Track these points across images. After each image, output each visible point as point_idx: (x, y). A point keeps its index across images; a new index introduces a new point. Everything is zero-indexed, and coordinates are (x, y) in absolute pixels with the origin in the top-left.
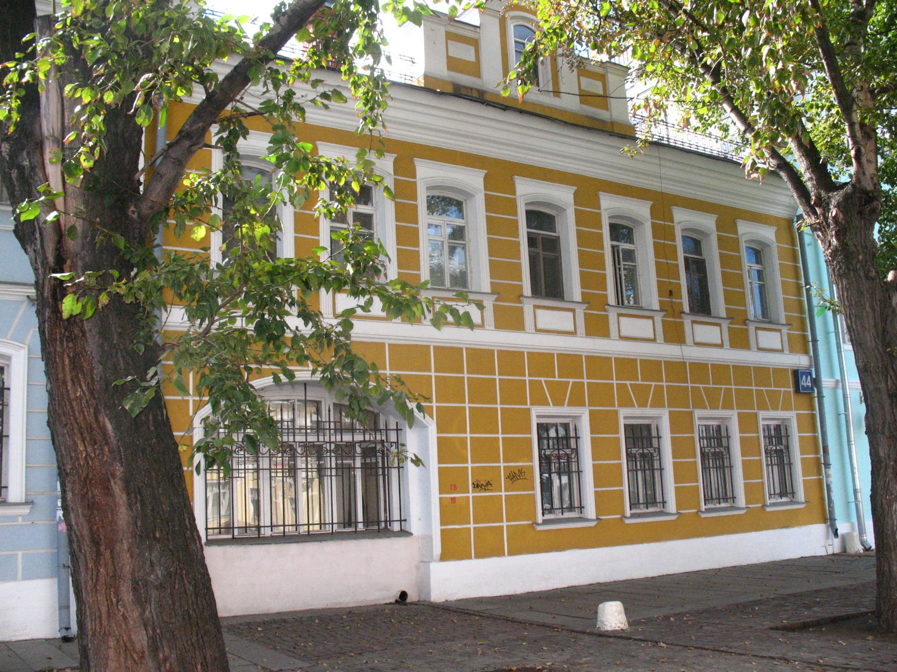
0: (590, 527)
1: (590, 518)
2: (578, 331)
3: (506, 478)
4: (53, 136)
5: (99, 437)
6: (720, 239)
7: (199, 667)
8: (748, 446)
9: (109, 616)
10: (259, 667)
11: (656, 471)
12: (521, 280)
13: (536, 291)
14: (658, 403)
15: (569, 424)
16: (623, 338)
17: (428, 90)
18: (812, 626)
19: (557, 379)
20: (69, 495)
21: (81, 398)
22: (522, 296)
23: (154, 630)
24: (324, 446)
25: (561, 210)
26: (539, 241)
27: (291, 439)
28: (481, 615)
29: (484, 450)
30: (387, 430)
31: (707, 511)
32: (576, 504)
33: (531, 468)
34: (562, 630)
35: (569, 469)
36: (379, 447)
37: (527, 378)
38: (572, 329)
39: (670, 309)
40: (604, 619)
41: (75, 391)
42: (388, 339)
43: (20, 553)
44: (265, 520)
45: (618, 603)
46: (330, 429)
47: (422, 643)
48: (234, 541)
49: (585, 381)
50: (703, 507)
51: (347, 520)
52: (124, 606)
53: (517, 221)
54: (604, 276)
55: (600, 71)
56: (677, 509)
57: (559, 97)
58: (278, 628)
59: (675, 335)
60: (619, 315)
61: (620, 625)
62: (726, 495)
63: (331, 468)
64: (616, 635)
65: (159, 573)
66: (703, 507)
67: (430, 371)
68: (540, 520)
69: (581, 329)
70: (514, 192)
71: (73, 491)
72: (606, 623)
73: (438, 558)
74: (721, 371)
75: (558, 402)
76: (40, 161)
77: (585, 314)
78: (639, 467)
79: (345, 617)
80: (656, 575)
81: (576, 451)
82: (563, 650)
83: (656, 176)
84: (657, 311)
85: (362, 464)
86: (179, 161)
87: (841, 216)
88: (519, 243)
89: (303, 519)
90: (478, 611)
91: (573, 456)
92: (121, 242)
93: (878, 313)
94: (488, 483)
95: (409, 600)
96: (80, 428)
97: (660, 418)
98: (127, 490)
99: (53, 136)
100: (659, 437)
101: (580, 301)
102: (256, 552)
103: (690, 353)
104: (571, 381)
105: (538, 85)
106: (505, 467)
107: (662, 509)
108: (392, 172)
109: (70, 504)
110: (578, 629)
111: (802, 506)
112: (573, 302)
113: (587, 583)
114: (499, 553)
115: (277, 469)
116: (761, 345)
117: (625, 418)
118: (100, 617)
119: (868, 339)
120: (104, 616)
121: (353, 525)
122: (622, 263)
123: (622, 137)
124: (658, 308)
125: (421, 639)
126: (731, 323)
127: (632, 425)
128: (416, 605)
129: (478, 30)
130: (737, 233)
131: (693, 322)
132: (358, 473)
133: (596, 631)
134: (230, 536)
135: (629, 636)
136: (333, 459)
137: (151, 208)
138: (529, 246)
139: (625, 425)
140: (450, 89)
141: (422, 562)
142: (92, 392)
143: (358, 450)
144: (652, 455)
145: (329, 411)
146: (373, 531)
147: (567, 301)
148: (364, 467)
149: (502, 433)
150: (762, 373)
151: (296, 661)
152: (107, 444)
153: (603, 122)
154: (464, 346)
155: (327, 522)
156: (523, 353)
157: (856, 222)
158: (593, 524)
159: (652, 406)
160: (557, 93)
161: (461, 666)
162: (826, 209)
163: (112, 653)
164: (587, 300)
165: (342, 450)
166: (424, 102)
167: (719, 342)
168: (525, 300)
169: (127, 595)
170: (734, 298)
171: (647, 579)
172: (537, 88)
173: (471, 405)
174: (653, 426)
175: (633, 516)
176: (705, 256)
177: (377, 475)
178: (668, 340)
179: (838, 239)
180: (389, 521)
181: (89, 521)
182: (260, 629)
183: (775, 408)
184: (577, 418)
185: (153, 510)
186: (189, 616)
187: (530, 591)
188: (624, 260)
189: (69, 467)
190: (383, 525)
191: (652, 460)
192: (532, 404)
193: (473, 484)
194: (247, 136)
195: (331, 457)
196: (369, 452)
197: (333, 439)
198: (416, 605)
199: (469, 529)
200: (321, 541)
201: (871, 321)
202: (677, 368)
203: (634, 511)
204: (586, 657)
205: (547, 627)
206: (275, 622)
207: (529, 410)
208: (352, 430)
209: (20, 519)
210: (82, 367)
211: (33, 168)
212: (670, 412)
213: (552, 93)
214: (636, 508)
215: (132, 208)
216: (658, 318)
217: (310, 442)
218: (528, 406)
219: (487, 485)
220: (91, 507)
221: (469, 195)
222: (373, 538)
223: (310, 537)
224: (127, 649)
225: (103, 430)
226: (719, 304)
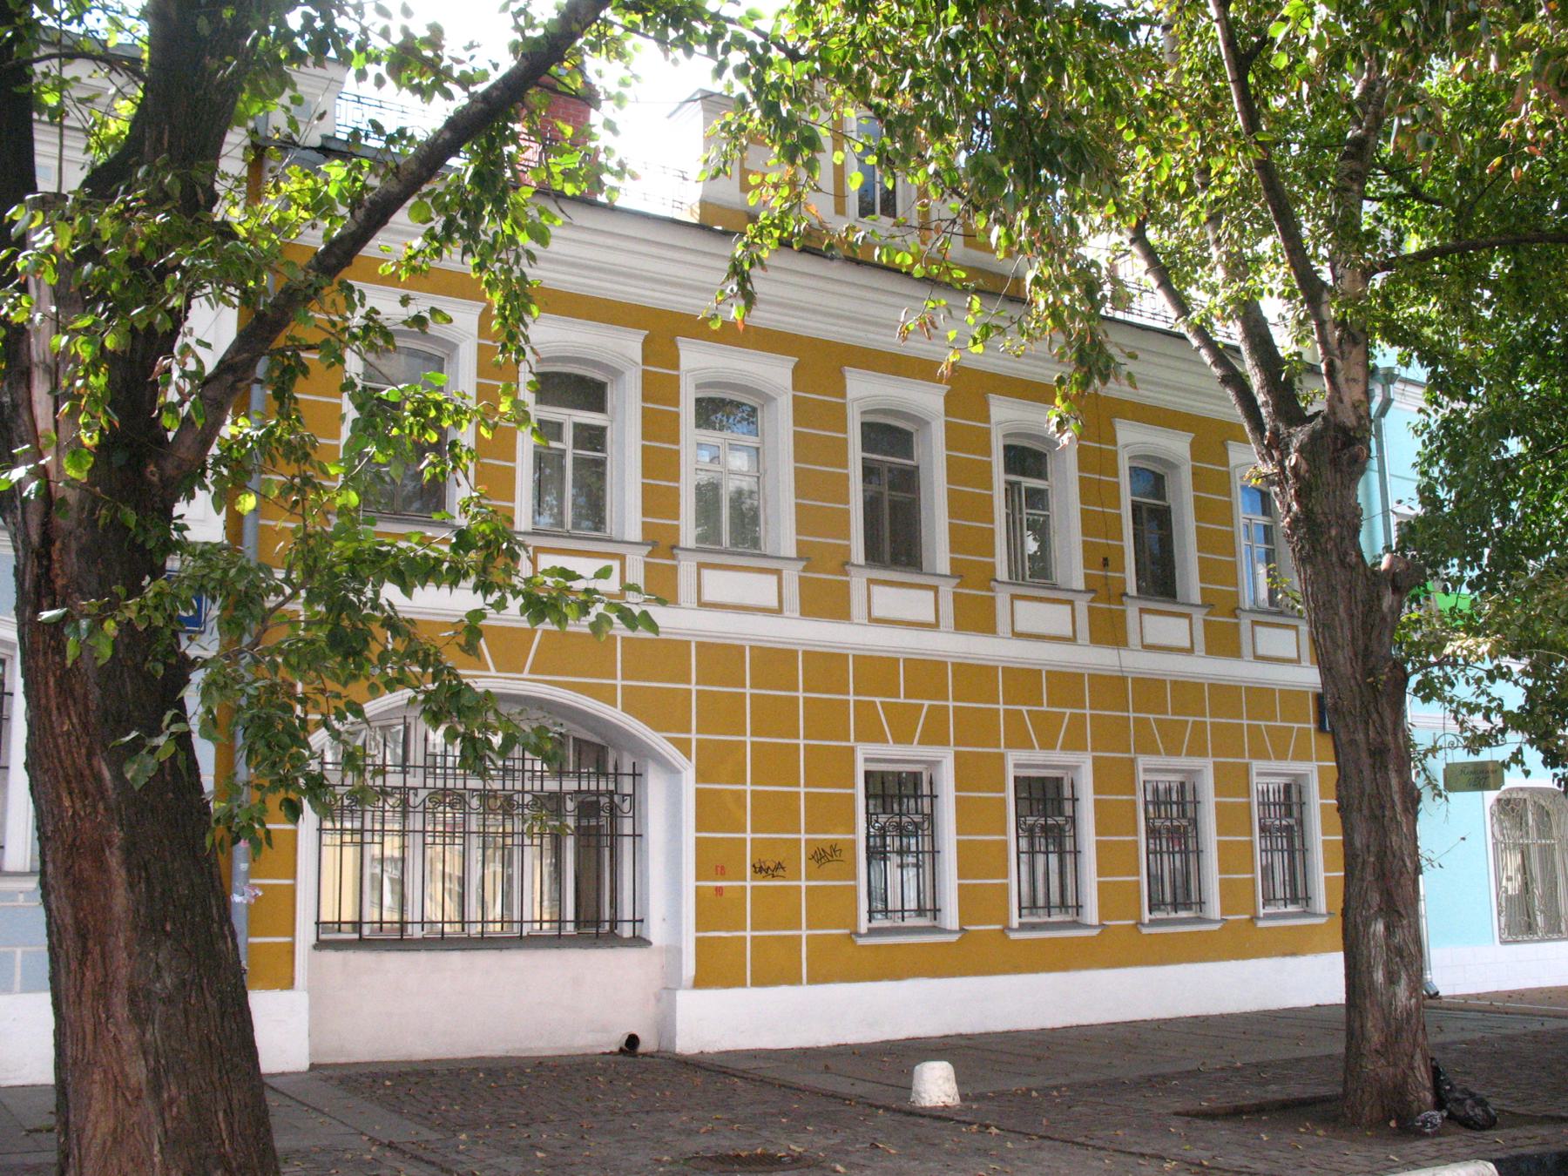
0: (949, 944)
2: (942, 624)
3: (811, 858)
4: (44, 362)
5: (91, 787)
6: (1196, 473)
7: (221, 1115)
8: (1229, 819)
9: (95, 1038)
14: (1074, 743)
17: (703, 227)
18: (1247, 1113)
19: (902, 700)
20: (50, 868)
21: (68, 733)
23: (157, 1062)
27: (460, 784)
28: (744, 1076)
29: (775, 812)
30: (616, 774)
31: (1153, 923)
32: (1071, 901)
33: (853, 844)
36: (604, 800)
38: (931, 618)
39: (1103, 589)
40: (921, 1089)
41: (62, 724)
43: (19, 951)
44: (413, 914)
46: (523, 771)
47: (628, 1114)
48: (363, 943)
49: (951, 704)
50: (1146, 917)
52: (116, 1025)
56: (1101, 919)
59: (1109, 631)
62: (1184, 895)
64: (939, 1116)
65: (168, 981)
66: (1146, 917)
67: (688, 681)
71: (54, 863)
74: (1188, 692)
75: (903, 737)
76: (25, 396)
81: (1073, 820)
87: (1304, 466)
88: (847, 477)
89: (474, 913)
92: (131, 518)
93: (1357, 622)
94: (779, 866)
95: (641, 1049)
96: (66, 775)
97: (1076, 768)
98: (127, 863)
99: (44, 362)
100: (1075, 800)
102: (395, 962)
103: (1134, 662)
105: (894, 216)
106: (807, 841)
108: (639, 359)
109: (51, 881)
111: (1322, 921)
112: (935, 575)
113: (941, 1033)
114: (794, 980)
116: (1261, 651)
117: (1017, 766)
118: (84, 1038)
119: (1342, 661)
120: (89, 1037)
122: (1025, 511)
126: (958, 586)
127: (1029, 779)
130: (1227, 464)
131: (1142, 611)
133: (907, 1107)
134: (356, 936)
137: (179, 467)
139: (1016, 778)
142: (85, 726)
143: (570, 805)
146: (588, 936)
150: (1261, 698)
152: (103, 798)
154: (747, 644)
157: (1328, 473)
158: (954, 938)
159: (1063, 748)
162: (1285, 454)
163: (96, 1089)
164: (959, 572)
167: (1187, 644)
168: (853, 571)
169: (121, 1011)
170: (1220, 571)
172: (891, 221)
176: (1170, 500)
178: (1097, 638)
179: (1299, 503)
180: (614, 922)
181: (73, 906)
183: (1281, 756)
185: (163, 893)
186: (210, 1044)
189: (50, 828)
190: (607, 926)
192: (856, 740)
196: (588, 806)
197: (528, 787)
199: (744, 938)
200: (501, 949)
201: (1348, 634)
202: (1110, 687)
206: (417, 1073)
207: (852, 750)
209: (21, 897)
210: (72, 691)
211: (15, 406)
212: (1095, 759)
215: (152, 468)
216: (1082, 604)
218: (852, 743)
220: (78, 885)
221: (768, 399)
223: (485, 942)
224: (117, 1085)
225: (98, 777)
226: (1190, 581)
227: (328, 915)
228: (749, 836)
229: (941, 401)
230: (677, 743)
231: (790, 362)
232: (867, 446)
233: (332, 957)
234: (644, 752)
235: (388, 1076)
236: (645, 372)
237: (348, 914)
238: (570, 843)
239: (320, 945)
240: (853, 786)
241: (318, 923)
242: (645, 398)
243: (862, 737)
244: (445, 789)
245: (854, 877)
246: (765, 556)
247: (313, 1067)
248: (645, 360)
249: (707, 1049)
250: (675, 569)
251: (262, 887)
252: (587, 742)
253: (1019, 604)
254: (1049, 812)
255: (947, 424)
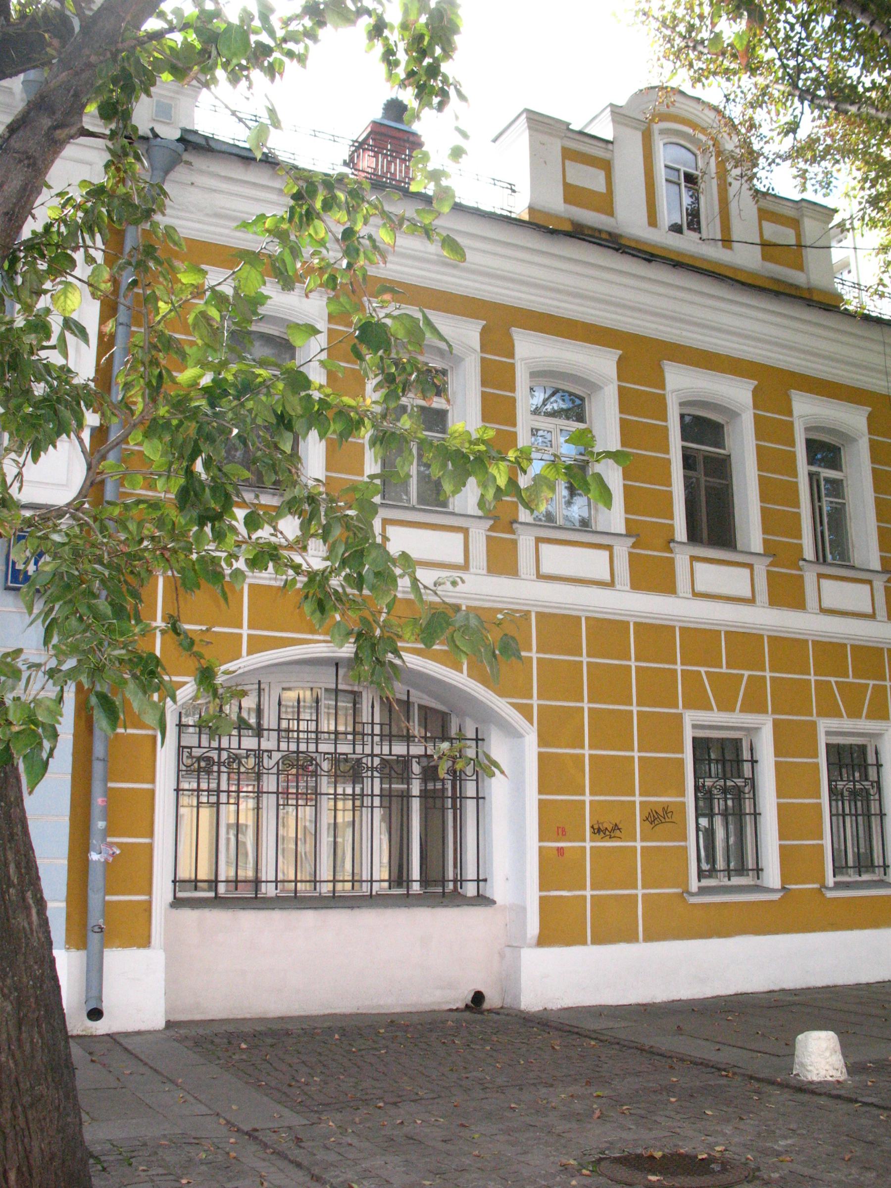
1: (771, 887)
3: (645, 820)
10: (222, 1121)
11: (873, 818)
12: (671, 517)
13: (694, 536)
15: (741, 739)
16: (824, 611)
22: (673, 540)
24: (364, 760)
25: (733, 414)
26: (700, 460)
34: (734, 1074)
35: (741, 810)
37: (679, 667)
40: (807, 1061)
42: (465, 598)
45: (831, 1034)
46: (373, 735)
48: (218, 902)
49: (768, 674)
51: (395, 876)
53: (666, 429)
54: (798, 516)
55: (791, 213)
57: (730, 248)
58: (272, 1046)
60: (820, 576)
61: (834, 1073)
63: (372, 795)
68: (694, 885)
69: (763, 595)
70: (662, 385)
72: (809, 1068)
73: (534, 941)
75: (726, 706)
77: (769, 573)
78: (859, 811)
79: (382, 1031)
80: (872, 981)
81: (752, 782)
82: (741, 1119)
83: (880, 372)
84: (877, 572)
85: (421, 791)
86: (28, 158)
88: (669, 461)
89: (325, 873)
90: (594, 1031)
91: (747, 790)
94: (616, 827)
95: (486, 1005)
101: (762, 552)
104: (747, 673)
107: (882, 877)
108: (477, 347)
110: (761, 1076)
114: (631, 938)
115: (307, 794)
117: (828, 733)
121: (405, 884)
122: (824, 499)
123: (825, 309)
124: (879, 568)
125: (500, 1080)
127: (838, 746)
128: (498, 1014)
129: (610, 147)
132: (416, 804)
134: (212, 894)
135: (853, 1096)
136: (377, 782)
138: (684, 468)
139: (828, 745)
140: (568, 227)
141: (509, 946)
143: (416, 768)
144: (867, 791)
145: (373, 707)
147: (742, 552)
148: (425, 795)
149: (639, 751)
151: (286, 1112)
153: (797, 287)
155: (364, 878)
156: (674, 627)
158: (776, 897)
160: (727, 242)
161: (563, 1141)
164: (771, 550)
165: (391, 768)
166: (530, 245)
171: (858, 986)
172: (700, 236)
173: (591, 705)
174: (869, 749)
175: (838, 886)
177: (443, 809)
180: (459, 881)
182: (244, 1046)
184: (753, 731)
187: (677, 997)
188: (827, 495)
190: (451, 886)
191: (868, 801)
192: (684, 707)
193: (592, 827)
194: (152, 89)
195: (372, 777)
196: (430, 773)
197: (377, 750)
198: (498, 1014)
199: (585, 897)
200: (352, 908)
203: (839, 878)
204: (785, 1137)
205: (707, 1066)
206: (272, 1033)
208: (408, 738)
212: (774, 720)
213: (720, 243)
214: (842, 874)
217: (341, 754)
218: (680, 710)
219: (613, 830)
222: (433, 906)
223: (334, 901)
227: (185, 873)
228: (587, 798)
229: (749, 395)
230: (517, 707)
231: (751, 384)
232: (686, 435)
233: (189, 915)
234: (487, 716)
235: (243, 1037)
236: (483, 359)
237: (204, 873)
238: (416, 804)
239: (177, 903)
240: (681, 750)
241: (174, 882)
242: (484, 383)
243: (687, 706)
244: (298, 752)
245: (684, 838)
246: (453, 514)
247: (169, 1024)
248: (483, 348)
249: (550, 1006)
250: (515, 543)
251: (119, 845)
252: (431, 709)
253: (544, 548)
254: (729, 775)
255: (756, 416)
